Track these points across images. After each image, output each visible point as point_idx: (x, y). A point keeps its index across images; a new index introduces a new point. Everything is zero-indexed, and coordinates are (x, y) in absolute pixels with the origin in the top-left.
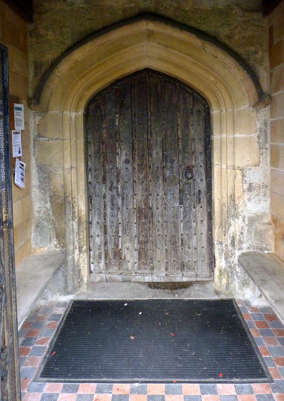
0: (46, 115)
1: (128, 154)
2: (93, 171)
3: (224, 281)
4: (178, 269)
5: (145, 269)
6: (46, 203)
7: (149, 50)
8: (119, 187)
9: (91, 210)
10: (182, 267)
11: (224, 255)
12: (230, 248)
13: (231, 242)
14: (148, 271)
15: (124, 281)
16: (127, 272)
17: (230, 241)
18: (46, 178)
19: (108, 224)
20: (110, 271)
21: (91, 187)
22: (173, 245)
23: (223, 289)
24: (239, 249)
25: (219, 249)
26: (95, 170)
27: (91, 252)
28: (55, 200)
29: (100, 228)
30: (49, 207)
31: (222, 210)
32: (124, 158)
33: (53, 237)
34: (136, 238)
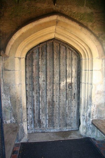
0: (8, 59)
1: (44, 77)
2: (28, 85)
3: (85, 131)
4: (64, 126)
5: (51, 127)
6: (8, 101)
7: (50, 29)
8: (40, 92)
9: (28, 103)
10: (66, 125)
11: (85, 120)
12: (88, 118)
13: (89, 115)
14: (52, 128)
15: (42, 133)
16: (43, 129)
17: (88, 115)
18: (8, 89)
19: (35, 108)
20: (36, 128)
21: (28, 93)
22: (63, 116)
23: (84, 134)
24: (92, 118)
25: (83, 118)
26: (29, 85)
27: (28, 121)
28: (12, 99)
29: (32, 110)
30: (10, 103)
31: (85, 102)
32: (42, 79)
33: (12, 117)
34: (48, 114)
